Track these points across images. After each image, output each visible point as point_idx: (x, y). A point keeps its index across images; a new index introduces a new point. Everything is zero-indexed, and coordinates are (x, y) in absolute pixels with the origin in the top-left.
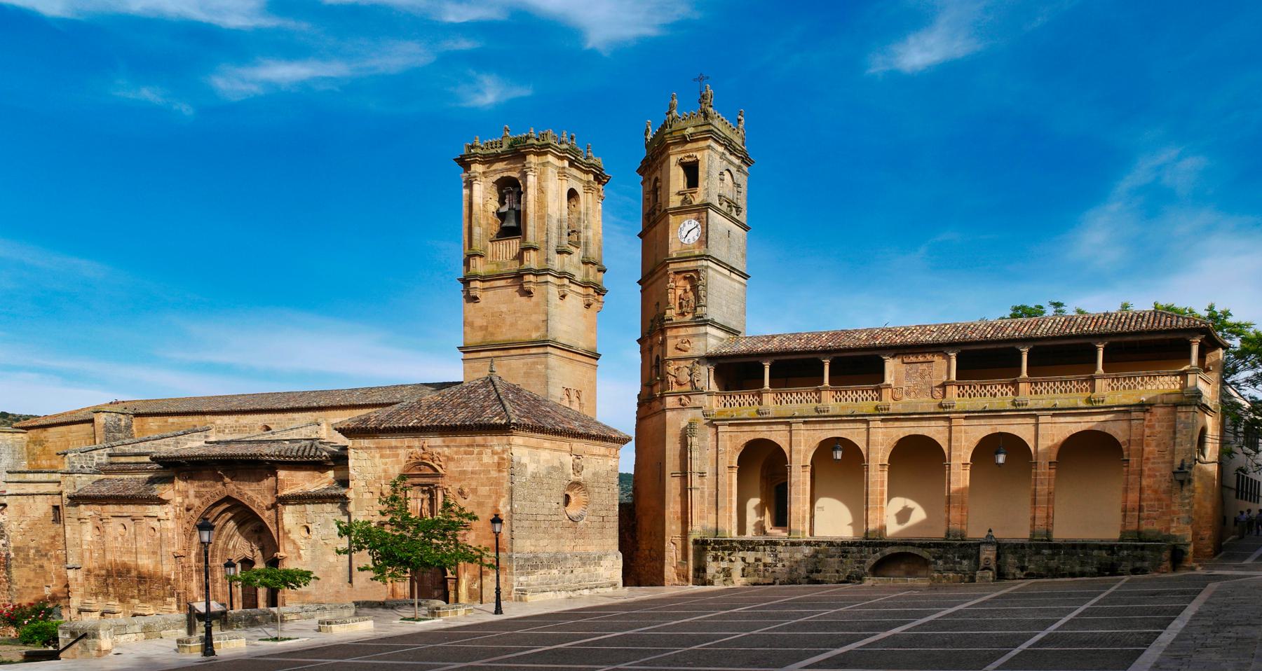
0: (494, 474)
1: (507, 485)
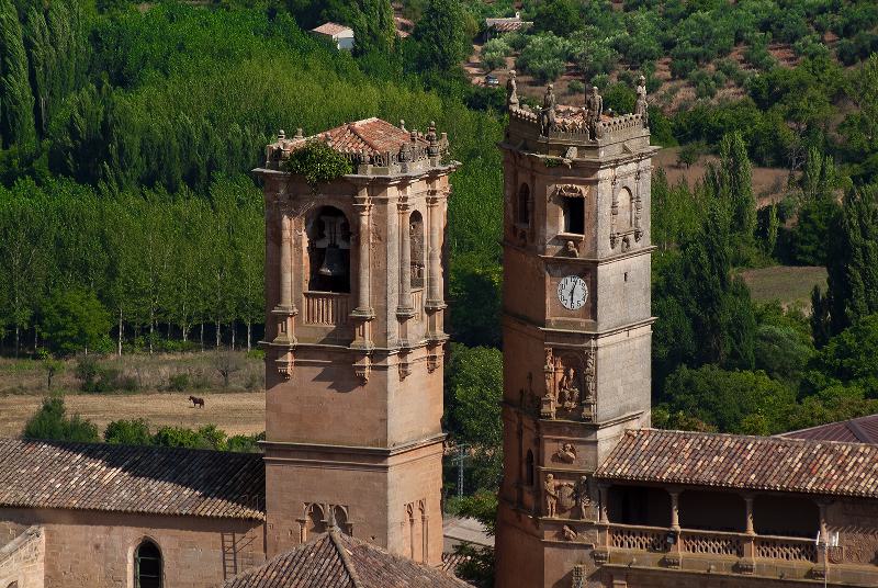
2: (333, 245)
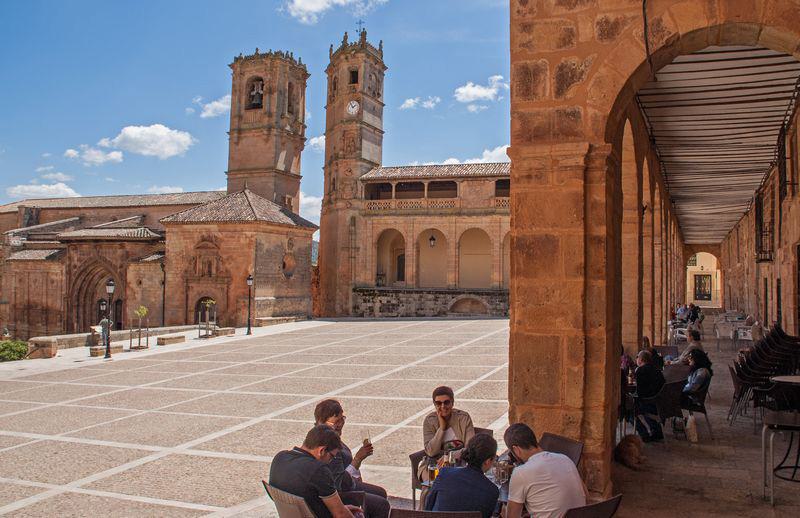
0: (246, 250)
1: (253, 256)
2: (258, 93)
